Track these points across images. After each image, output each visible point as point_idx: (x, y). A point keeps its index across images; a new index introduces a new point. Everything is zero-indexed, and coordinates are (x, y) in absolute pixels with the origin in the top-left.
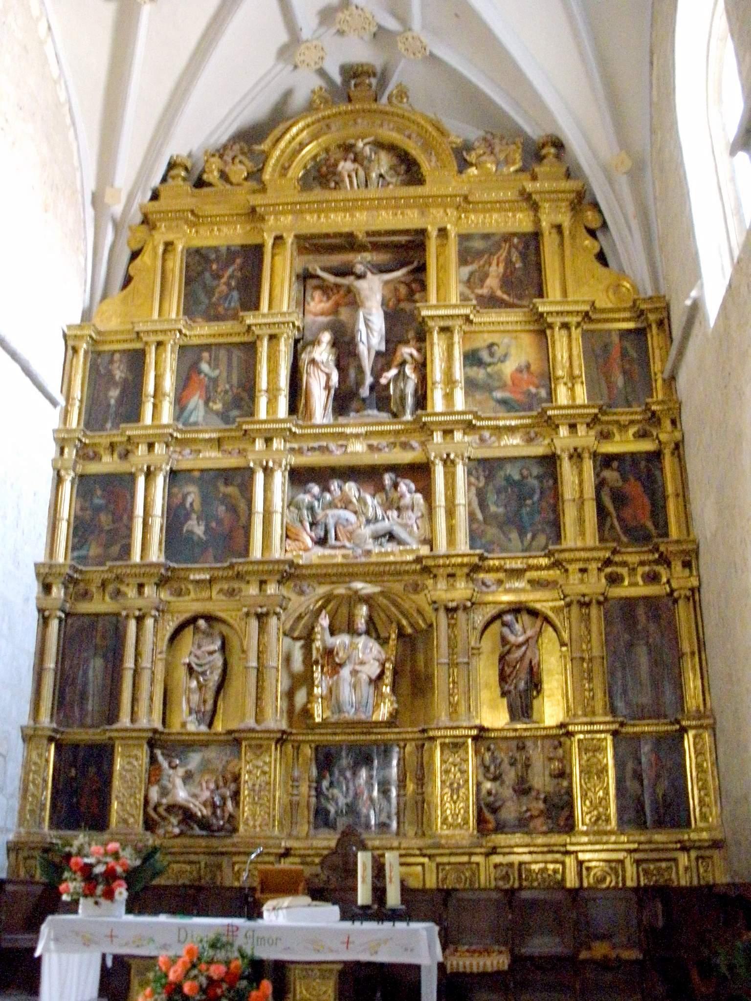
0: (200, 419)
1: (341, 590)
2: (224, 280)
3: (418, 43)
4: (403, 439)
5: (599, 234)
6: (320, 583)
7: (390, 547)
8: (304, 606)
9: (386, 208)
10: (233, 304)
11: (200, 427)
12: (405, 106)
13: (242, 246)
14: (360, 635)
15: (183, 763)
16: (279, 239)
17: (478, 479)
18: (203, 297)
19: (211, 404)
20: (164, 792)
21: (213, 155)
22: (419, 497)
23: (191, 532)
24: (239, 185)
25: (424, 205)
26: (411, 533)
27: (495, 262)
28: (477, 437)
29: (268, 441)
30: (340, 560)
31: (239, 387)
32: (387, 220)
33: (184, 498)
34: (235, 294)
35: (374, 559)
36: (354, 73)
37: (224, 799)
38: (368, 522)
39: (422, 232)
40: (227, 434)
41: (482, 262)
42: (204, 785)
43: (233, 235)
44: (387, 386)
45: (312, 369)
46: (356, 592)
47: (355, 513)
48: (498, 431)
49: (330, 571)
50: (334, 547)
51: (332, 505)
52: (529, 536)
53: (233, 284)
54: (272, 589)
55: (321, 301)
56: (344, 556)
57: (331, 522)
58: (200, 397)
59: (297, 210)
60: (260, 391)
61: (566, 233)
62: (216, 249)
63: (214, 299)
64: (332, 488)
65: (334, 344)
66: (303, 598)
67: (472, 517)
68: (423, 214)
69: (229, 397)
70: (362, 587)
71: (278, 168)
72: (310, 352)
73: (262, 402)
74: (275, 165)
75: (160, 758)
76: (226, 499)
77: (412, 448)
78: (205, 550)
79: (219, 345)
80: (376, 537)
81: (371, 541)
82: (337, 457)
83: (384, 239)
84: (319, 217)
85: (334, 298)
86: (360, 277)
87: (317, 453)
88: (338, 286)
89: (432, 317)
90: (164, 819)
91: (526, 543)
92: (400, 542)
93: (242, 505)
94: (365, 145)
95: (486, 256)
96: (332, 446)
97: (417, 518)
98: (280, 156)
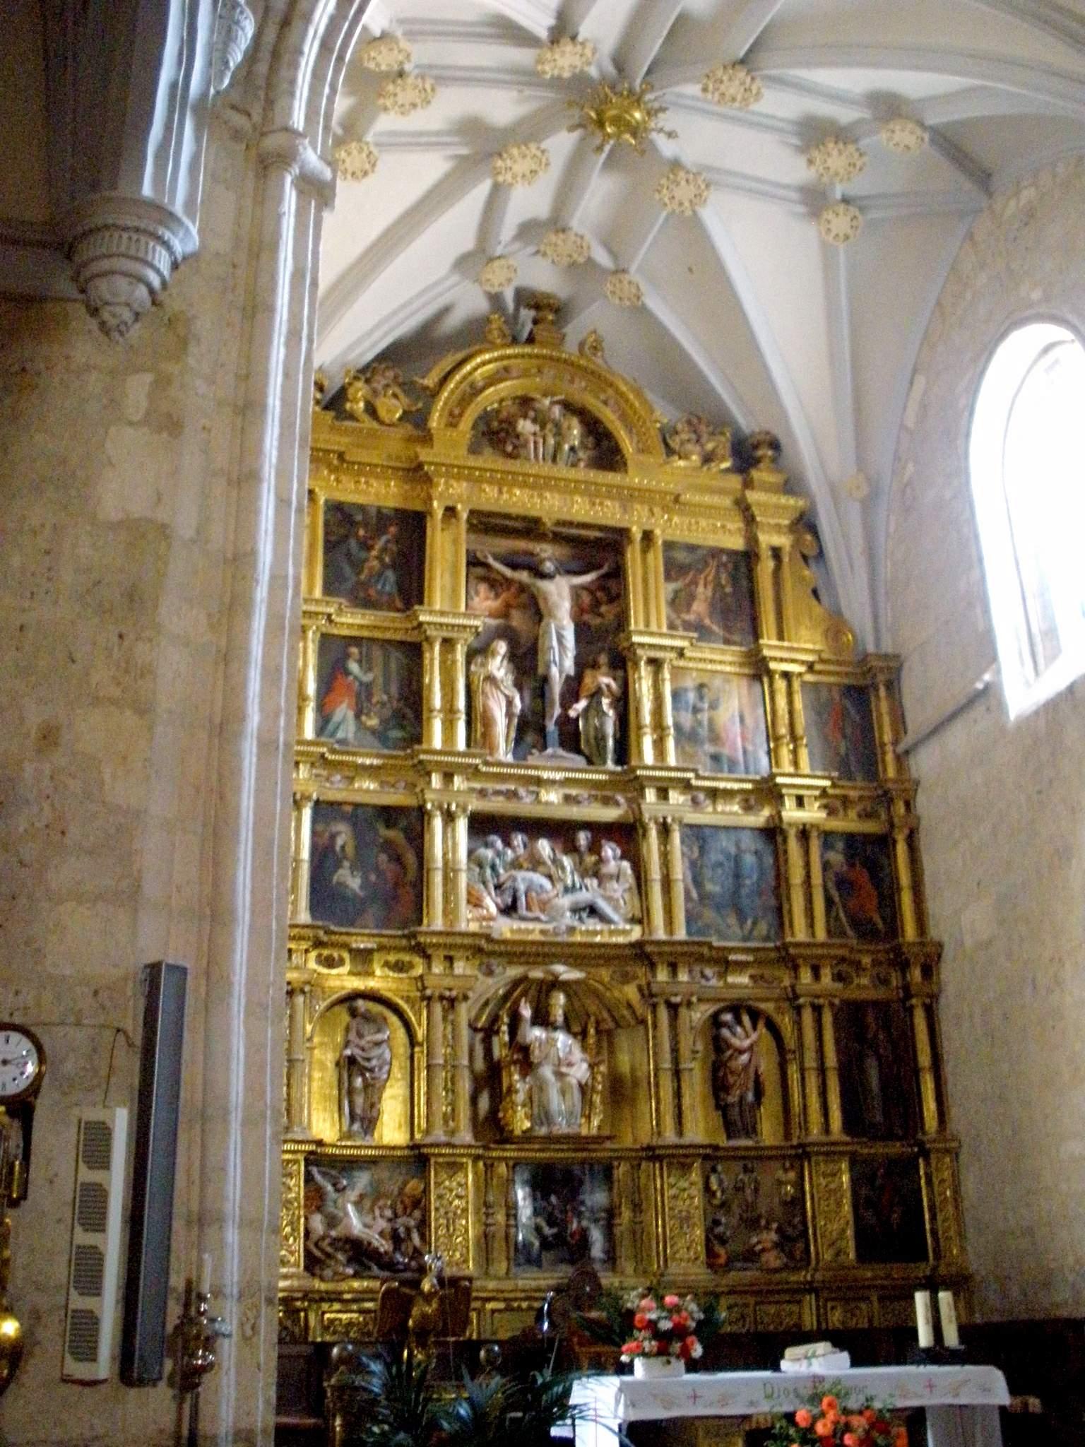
0: (351, 736)
1: (537, 974)
2: (374, 553)
3: (634, 290)
4: (608, 793)
5: (811, 561)
6: (510, 963)
7: (593, 924)
8: (493, 991)
9: (582, 494)
10: (388, 588)
11: (350, 749)
12: (600, 361)
13: (397, 510)
14: (555, 1028)
15: (352, 1186)
16: (450, 511)
17: (691, 849)
18: (347, 570)
19: (364, 718)
20: (332, 1222)
21: (356, 378)
22: (626, 865)
23: (341, 884)
25: (628, 497)
26: (616, 908)
27: (702, 582)
28: (689, 797)
29: (448, 777)
30: (537, 937)
31: (399, 700)
32: (580, 509)
33: (333, 837)
34: (390, 575)
35: (578, 938)
36: (530, 299)
37: (408, 1230)
38: (567, 890)
39: (623, 533)
40: (391, 762)
41: (687, 581)
42: (377, 1212)
43: (383, 493)
44: (577, 719)
45: (488, 687)
46: (556, 976)
47: (550, 877)
48: (714, 794)
49: (528, 949)
50: (523, 919)
51: (516, 865)
52: (749, 922)
53: (387, 559)
54: (460, 967)
55: (487, 598)
56: (543, 932)
57: (522, 887)
58: (349, 706)
59: (474, 478)
60: (431, 711)
61: (786, 559)
62: (362, 508)
63: (363, 577)
64: (516, 843)
65: (512, 657)
66: (490, 981)
67: (688, 897)
68: (625, 509)
69: (387, 712)
70: (566, 973)
71: (446, 413)
72: (483, 665)
73: (437, 726)
74: (443, 409)
75: (318, 1177)
76: (388, 846)
77: (617, 804)
78: (360, 912)
79: (372, 640)
80: (576, 910)
81: (568, 914)
82: (525, 807)
83: (574, 531)
84: (500, 492)
85: (504, 595)
86: (549, 577)
87: (501, 798)
88: (509, 582)
89: (642, 645)
90: (329, 1256)
91: (746, 932)
92: (604, 919)
93: (410, 858)
94: (553, 403)
95: (691, 574)
96: (522, 792)
97: (625, 891)
98: (448, 398)
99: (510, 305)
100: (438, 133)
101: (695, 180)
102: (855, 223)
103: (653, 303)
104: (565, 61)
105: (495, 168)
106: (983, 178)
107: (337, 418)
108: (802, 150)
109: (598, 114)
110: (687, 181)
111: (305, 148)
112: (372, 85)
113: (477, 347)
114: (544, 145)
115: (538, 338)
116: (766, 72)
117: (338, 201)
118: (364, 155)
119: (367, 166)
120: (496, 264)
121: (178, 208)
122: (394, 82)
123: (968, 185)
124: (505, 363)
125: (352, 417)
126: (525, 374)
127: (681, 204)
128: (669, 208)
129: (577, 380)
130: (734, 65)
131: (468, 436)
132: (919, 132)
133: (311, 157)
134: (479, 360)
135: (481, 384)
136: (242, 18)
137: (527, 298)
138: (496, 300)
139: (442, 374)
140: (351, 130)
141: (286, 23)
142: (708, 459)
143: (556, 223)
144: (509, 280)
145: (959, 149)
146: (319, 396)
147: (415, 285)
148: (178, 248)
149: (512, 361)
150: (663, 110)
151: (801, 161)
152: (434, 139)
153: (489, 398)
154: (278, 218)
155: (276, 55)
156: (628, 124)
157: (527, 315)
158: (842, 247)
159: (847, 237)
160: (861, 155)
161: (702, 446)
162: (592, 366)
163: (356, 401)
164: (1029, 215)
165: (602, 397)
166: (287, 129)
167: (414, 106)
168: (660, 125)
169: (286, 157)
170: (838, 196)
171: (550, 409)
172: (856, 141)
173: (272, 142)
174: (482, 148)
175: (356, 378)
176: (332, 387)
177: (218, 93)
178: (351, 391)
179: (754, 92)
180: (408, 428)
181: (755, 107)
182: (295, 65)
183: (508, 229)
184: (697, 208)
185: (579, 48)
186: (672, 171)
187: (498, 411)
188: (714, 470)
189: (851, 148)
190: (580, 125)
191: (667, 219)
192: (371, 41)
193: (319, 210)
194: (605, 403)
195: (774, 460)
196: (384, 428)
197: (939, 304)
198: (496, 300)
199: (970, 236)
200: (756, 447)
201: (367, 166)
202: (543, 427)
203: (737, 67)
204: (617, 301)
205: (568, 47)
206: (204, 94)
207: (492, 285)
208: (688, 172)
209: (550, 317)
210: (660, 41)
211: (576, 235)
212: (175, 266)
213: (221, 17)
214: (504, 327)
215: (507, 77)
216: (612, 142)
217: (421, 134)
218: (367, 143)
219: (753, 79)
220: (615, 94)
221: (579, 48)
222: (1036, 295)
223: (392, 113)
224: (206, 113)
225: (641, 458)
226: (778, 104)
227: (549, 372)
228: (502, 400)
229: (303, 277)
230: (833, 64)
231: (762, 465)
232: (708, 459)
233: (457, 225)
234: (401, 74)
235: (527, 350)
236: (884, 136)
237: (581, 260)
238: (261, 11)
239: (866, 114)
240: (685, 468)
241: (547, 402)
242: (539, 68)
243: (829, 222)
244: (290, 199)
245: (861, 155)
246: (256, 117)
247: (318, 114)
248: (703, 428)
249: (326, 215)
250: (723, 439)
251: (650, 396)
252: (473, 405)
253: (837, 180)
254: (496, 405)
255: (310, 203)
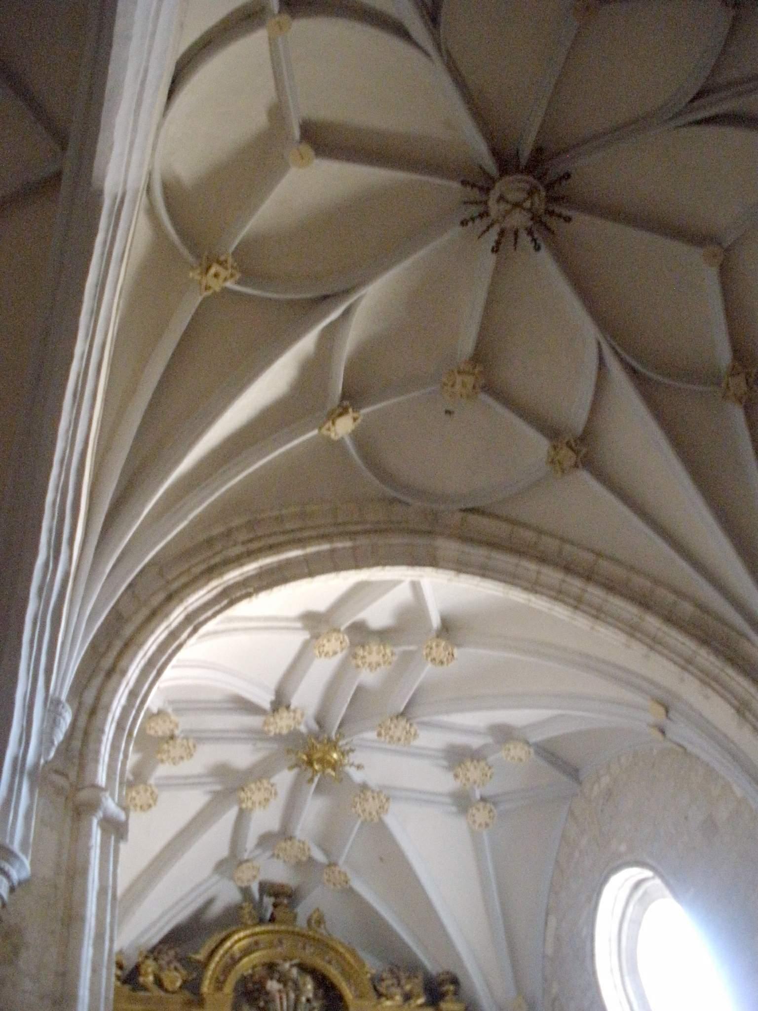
3: (343, 878)
12: (323, 931)
21: (147, 957)
24: (173, 992)
94: (292, 966)
98: (215, 968)
99: (257, 895)
100: (199, 776)
101: (379, 797)
102: (491, 814)
103: (358, 885)
104: (283, 723)
105: (240, 799)
106: (573, 772)
107: (134, 990)
108: (450, 768)
109: (308, 756)
110: (373, 798)
111: (106, 799)
112: (154, 746)
113: (234, 928)
114: (273, 780)
115: (278, 918)
116: (418, 720)
117: (131, 835)
118: (148, 794)
119: (151, 802)
120: (244, 866)
121: (16, 847)
122: (167, 743)
123: (564, 779)
124: (256, 938)
125: (144, 988)
126: (271, 945)
127: (370, 814)
128: (362, 818)
129: (307, 947)
130: (397, 717)
131: (231, 996)
132: (526, 748)
133: (110, 805)
134: (236, 937)
135: (238, 955)
136: (63, 711)
137: (267, 888)
138: (245, 891)
139: (210, 950)
140: (140, 776)
141: (93, 712)
142: (407, 997)
143: (285, 834)
144: (255, 877)
145: (553, 754)
146: (119, 973)
147: (186, 886)
148: (15, 875)
149: (262, 937)
150: (352, 750)
151: (450, 776)
152: (196, 780)
153: (245, 966)
154: (88, 849)
155: (86, 733)
156: (329, 762)
157: (268, 901)
158: (485, 833)
159: (487, 825)
160: (490, 768)
161: (402, 988)
162: (317, 936)
163: (146, 974)
164: (609, 794)
165: (327, 958)
166: (95, 786)
167: (182, 758)
168: (351, 761)
169: (93, 806)
170: (478, 797)
171: (289, 970)
172: (485, 758)
173: (84, 795)
174: (230, 785)
175: (147, 957)
176: (129, 965)
177: (46, 762)
178: (143, 967)
179: (413, 733)
180: (187, 995)
181: (416, 743)
182: (99, 741)
183: (251, 841)
184: (382, 816)
185: (292, 714)
186: (362, 791)
187: (252, 976)
188: (413, 1005)
189: (482, 764)
190: (296, 765)
191: (361, 828)
192: (150, 716)
193: (117, 842)
194: (330, 962)
195: (456, 993)
196: (168, 995)
197: (557, 862)
198: (245, 891)
199: (571, 813)
200: (441, 984)
201: (151, 802)
202: (285, 985)
203: (400, 718)
204: (332, 887)
205: (284, 714)
206: (36, 765)
207: (242, 882)
208: (373, 791)
209: (285, 901)
210: (346, 706)
211: (299, 841)
212: (12, 889)
213: (49, 711)
214: (253, 912)
215: (245, 735)
216: (319, 775)
217: (187, 777)
218: (150, 786)
219: (411, 725)
220: (320, 742)
221: (292, 714)
222: (623, 848)
223: (167, 764)
224: (39, 777)
225: (359, 1002)
226: (430, 740)
227: (287, 943)
228: (254, 967)
229: (106, 893)
230: (462, 710)
231: (447, 998)
232: (407, 997)
233: (215, 840)
234: (172, 737)
235: (270, 927)
236: (503, 754)
237: (304, 859)
238: (76, 705)
239: (489, 740)
240: (391, 1007)
241: (287, 965)
242: (266, 729)
243: (474, 816)
244: (96, 834)
245: (490, 768)
246: (73, 775)
247: (115, 774)
248: (403, 975)
249: (122, 846)
250: (416, 981)
251: (362, 954)
252: (233, 973)
253: (476, 786)
254: (250, 971)
255: (110, 838)
